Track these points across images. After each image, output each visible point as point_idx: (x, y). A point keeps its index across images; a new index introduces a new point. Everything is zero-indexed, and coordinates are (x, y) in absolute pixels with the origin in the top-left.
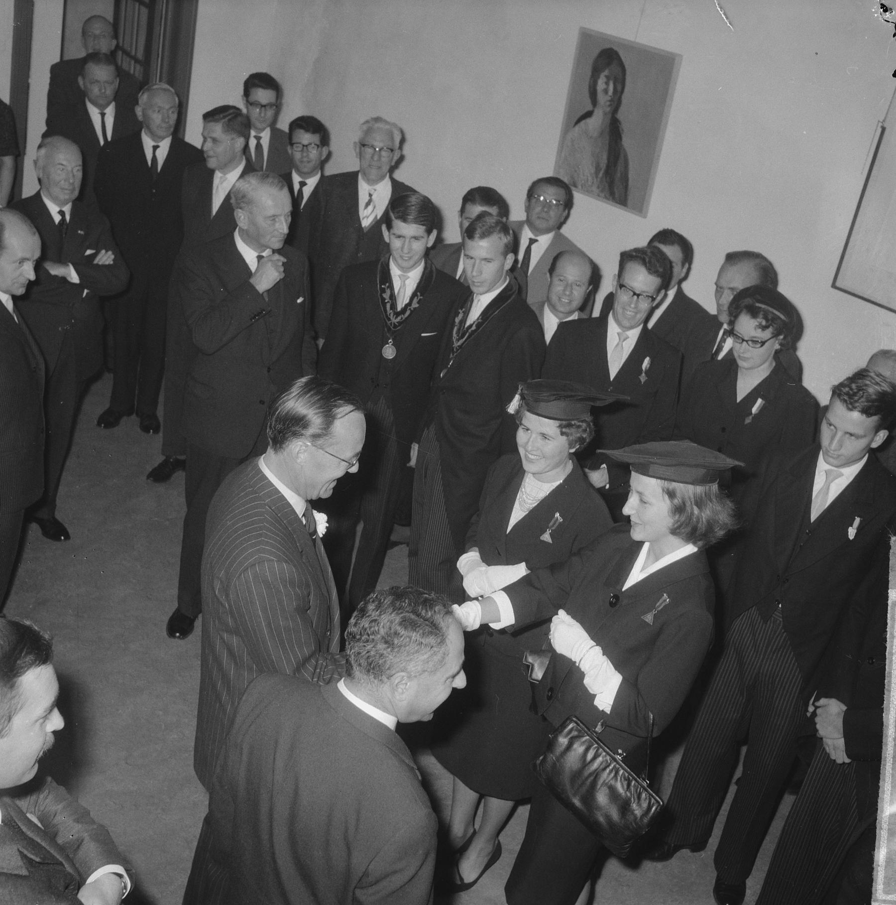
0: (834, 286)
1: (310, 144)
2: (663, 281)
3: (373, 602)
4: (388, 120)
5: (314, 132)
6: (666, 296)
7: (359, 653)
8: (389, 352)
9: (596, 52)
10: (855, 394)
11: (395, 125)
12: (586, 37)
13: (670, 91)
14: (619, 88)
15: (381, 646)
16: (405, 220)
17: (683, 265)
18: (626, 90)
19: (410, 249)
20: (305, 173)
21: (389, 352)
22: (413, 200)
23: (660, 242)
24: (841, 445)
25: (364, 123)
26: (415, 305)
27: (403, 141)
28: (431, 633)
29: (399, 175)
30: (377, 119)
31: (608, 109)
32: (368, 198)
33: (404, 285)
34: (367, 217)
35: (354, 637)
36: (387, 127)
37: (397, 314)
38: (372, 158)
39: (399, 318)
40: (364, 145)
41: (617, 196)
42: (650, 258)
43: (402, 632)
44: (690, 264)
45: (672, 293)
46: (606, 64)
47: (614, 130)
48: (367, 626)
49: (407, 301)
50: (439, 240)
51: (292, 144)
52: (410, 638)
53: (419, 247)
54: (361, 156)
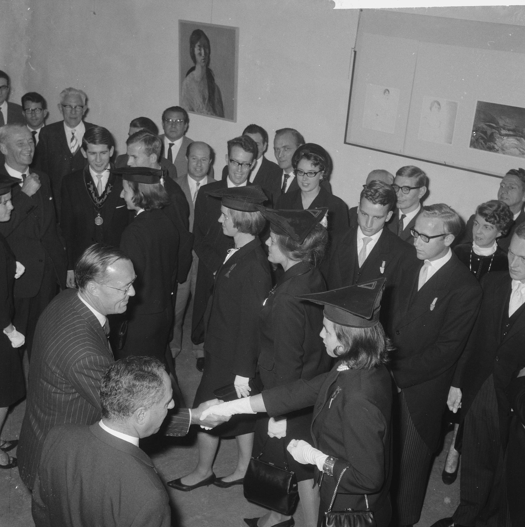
0: (345, 142)
1: (36, 109)
2: (254, 155)
3: (113, 370)
4: (76, 88)
5: (37, 102)
6: (256, 163)
7: (112, 403)
8: (99, 221)
9: (191, 33)
10: (375, 195)
11: (81, 91)
12: (183, 25)
13: (236, 49)
14: (207, 51)
15: (125, 396)
16: (95, 143)
17: (264, 143)
18: (212, 51)
19: (101, 160)
20: (35, 126)
21: (99, 221)
22: (96, 130)
23: (249, 132)
24: (372, 222)
25: (62, 92)
26: (109, 191)
27: (87, 100)
28: (153, 380)
29: (87, 120)
30: (70, 89)
31: (204, 64)
32: (71, 136)
33: (100, 181)
34: (73, 147)
35: (107, 394)
36: (77, 93)
37: (100, 198)
38: (71, 112)
39: (101, 201)
40: (65, 106)
41: (218, 113)
42: (244, 143)
43: (138, 383)
44: (267, 142)
45: (260, 161)
46: (197, 38)
47: (209, 76)
48: (114, 385)
49: (104, 190)
50: (115, 153)
51: (25, 110)
52: (143, 385)
53: (105, 157)
54: (64, 112)
